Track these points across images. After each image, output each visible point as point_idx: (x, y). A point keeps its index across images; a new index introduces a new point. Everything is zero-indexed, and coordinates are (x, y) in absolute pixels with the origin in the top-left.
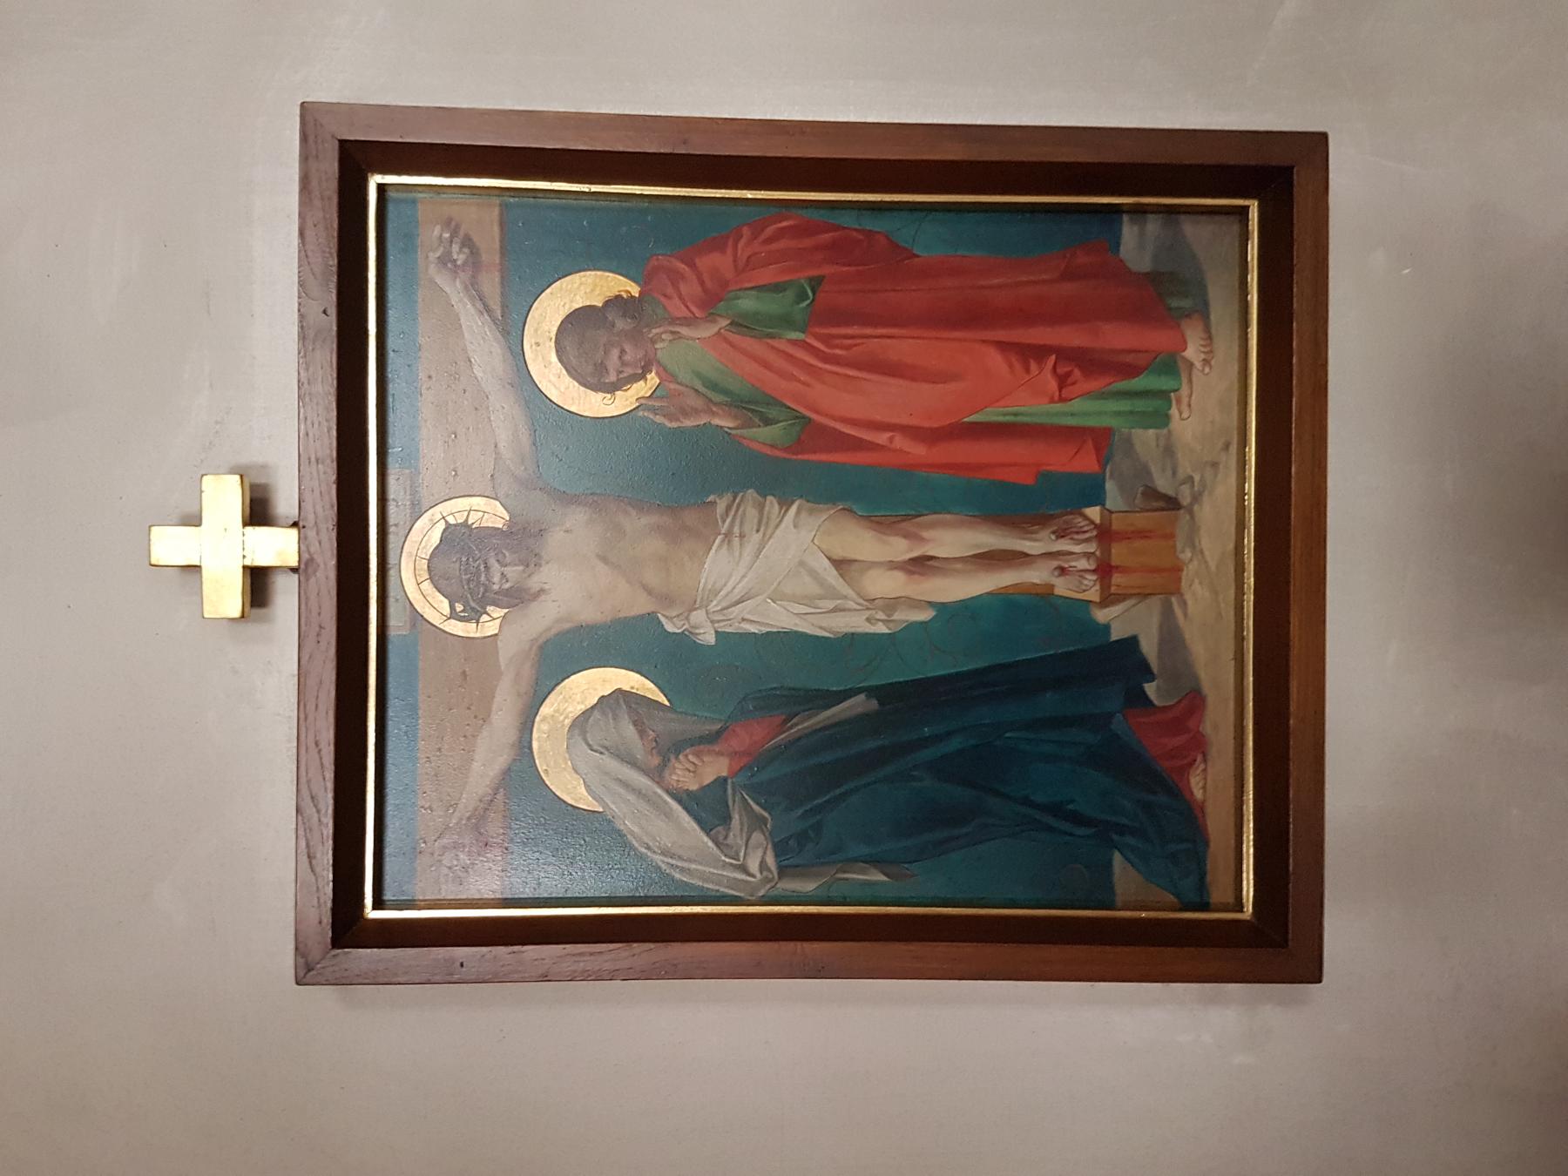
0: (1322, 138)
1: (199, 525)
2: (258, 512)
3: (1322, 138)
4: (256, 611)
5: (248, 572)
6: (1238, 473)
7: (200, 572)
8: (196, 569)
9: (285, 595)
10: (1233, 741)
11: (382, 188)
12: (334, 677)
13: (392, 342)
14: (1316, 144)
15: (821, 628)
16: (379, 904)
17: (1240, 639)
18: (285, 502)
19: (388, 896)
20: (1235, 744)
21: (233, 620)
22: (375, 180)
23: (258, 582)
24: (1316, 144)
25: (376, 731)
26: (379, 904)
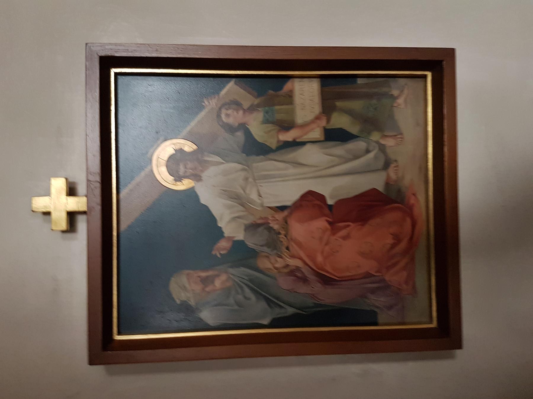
2: (71, 191)
9: (82, 224)
11: (116, 74)
14: (450, 53)
18: (82, 188)
21: (63, 232)
22: (113, 71)
23: (72, 216)
24: (450, 53)
26: (119, 333)
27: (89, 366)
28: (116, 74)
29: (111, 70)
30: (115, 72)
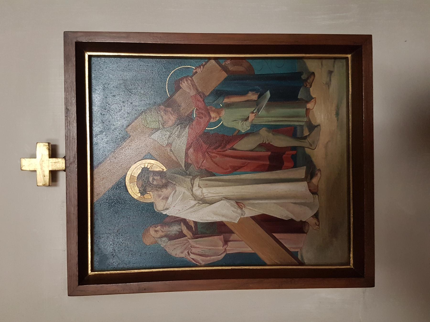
0: (371, 36)
1: (36, 158)
3: (371, 36)
4: (54, 183)
5: (50, 171)
6: (346, 67)
7: (36, 172)
8: (35, 171)
9: (62, 177)
10: (346, 116)
11: (90, 57)
12: (76, 186)
13: (96, 229)
14: (368, 39)
15: (223, 216)
16: (92, 271)
17: (348, 140)
18: (62, 150)
19: (96, 264)
20: (346, 116)
23: (54, 174)
24: (368, 39)
25: (91, 249)
27: (375, 287)
28: (90, 57)
29: (86, 54)
30: (89, 54)
